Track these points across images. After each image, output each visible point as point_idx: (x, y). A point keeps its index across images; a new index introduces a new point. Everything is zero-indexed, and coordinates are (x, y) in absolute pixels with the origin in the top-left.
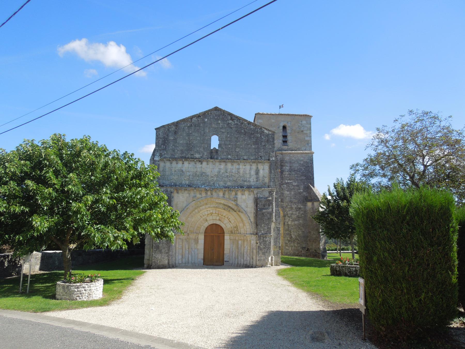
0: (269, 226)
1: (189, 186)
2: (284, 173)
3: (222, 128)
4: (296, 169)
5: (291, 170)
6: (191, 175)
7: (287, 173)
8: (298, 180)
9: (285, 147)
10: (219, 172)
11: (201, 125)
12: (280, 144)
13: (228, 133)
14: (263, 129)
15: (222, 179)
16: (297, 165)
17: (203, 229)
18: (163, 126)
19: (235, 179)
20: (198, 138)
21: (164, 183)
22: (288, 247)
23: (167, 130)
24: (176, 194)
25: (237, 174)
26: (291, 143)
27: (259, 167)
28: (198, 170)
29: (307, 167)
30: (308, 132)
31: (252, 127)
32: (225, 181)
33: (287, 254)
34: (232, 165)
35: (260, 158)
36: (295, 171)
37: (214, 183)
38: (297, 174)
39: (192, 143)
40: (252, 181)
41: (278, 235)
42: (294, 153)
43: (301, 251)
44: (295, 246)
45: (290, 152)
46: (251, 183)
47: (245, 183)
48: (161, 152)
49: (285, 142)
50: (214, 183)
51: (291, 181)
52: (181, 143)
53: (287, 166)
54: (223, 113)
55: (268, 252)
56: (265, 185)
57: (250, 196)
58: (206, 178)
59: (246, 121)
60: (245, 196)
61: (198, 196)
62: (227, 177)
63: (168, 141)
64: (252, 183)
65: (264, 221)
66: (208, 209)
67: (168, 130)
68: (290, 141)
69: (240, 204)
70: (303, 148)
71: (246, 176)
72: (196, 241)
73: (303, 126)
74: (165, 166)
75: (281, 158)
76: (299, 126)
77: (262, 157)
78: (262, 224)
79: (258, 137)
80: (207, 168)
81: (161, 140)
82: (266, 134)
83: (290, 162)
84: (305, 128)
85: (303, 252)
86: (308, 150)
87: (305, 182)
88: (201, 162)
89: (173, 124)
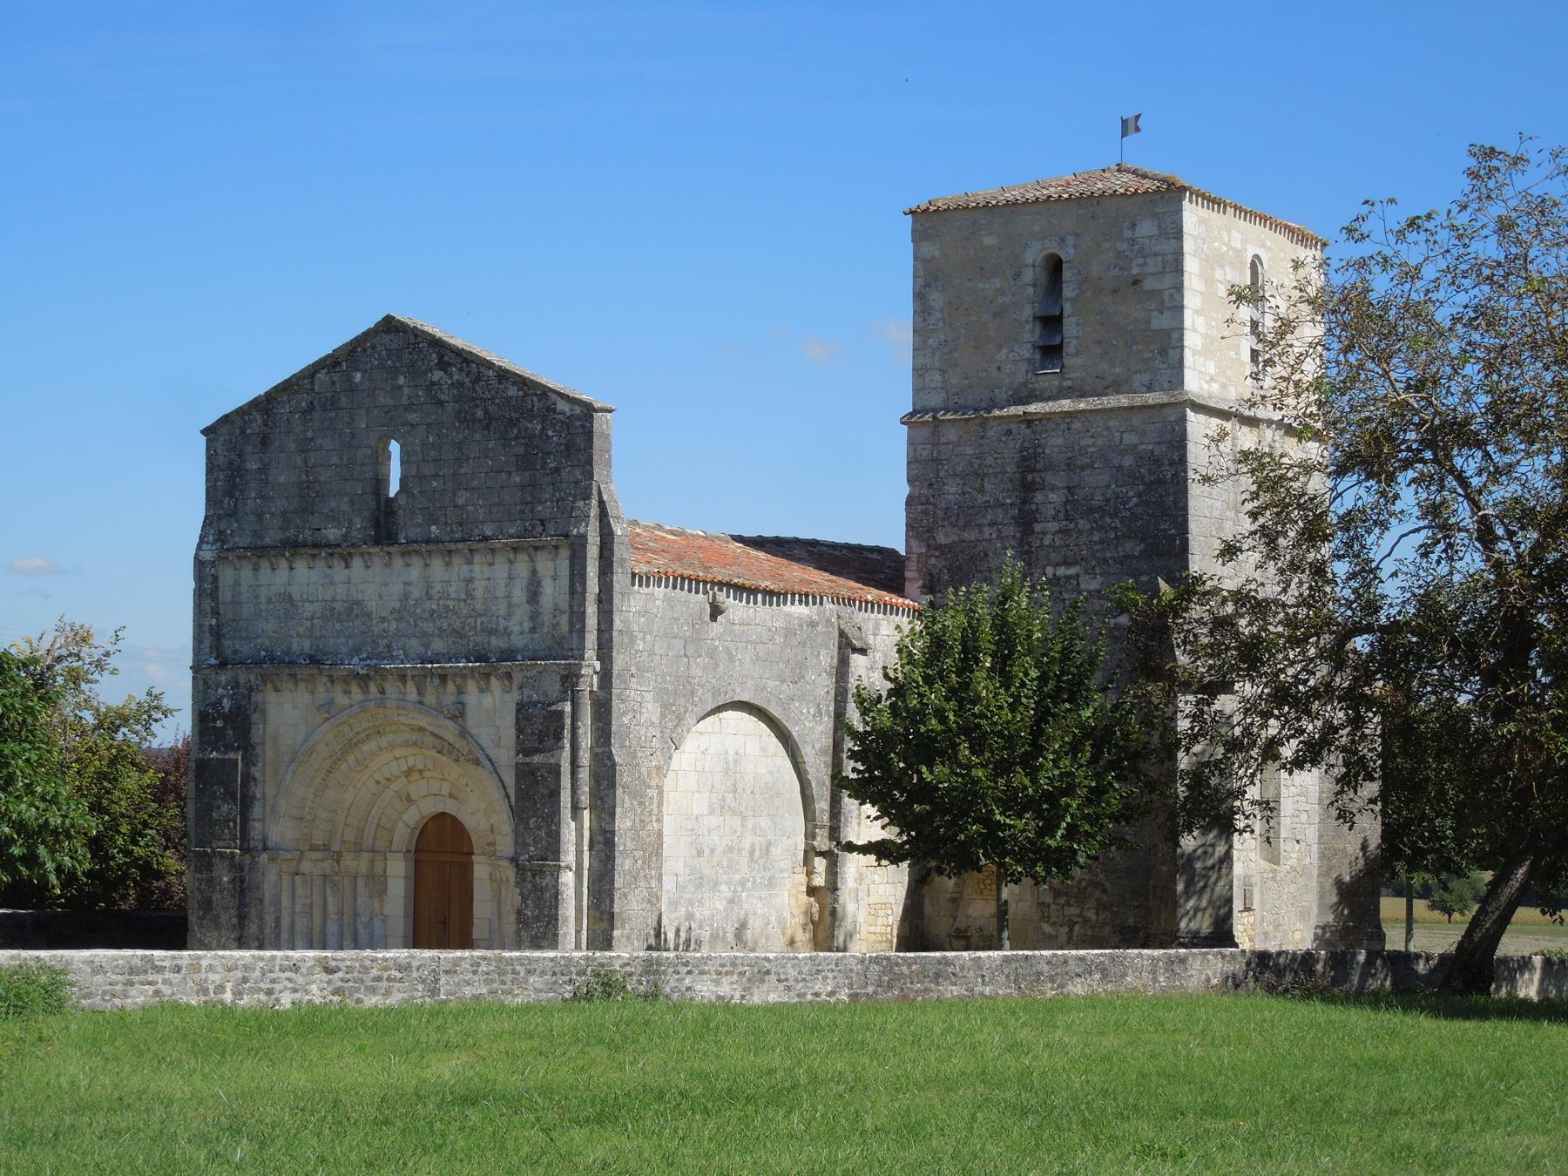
0: (554, 828)
1: (314, 661)
2: (1038, 527)
3: (408, 408)
4: (1098, 499)
5: (1070, 510)
6: (318, 615)
7: (1053, 526)
8: (1106, 561)
9: (1050, 376)
10: (406, 597)
11: (344, 400)
12: (1024, 367)
13: (429, 425)
14: (553, 396)
15: (416, 626)
17: (403, 836)
18: (225, 419)
19: (457, 625)
20: (335, 460)
21: (235, 652)
22: (1054, 924)
23: (237, 432)
24: (274, 693)
25: (465, 601)
26: (1077, 353)
27: (539, 569)
28: (339, 591)
29: (1152, 483)
30: (1168, 281)
31: (512, 391)
32: (424, 634)
34: (447, 564)
35: (539, 529)
36: (1091, 510)
37: (389, 646)
38: (1102, 528)
39: (316, 480)
40: (516, 629)
41: (606, 866)
44: (1086, 921)
45: (1066, 404)
46: (512, 637)
48: (223, 526)
50: (389, 646)
51: (1072, 571)
52: (280, 484)
54: (412, 340)
56: (563, 648)
57: (508, 697)
58: (363, 624)
59: (490, 365)
60: (492, 695)
61: (341, 699)
62: (432, 615)
63: (241, 477)
64: (518, 641)
65: (535, 803)
66: (398, 752)
67: (243, 432)
68: (1074, 342)
69: (474, 731)
70: (1137, 380)
71: (494, 608)
72: (378, 884)
73: (1141, 251)
74: (237, 584)
75: (1026, 444)
78: (529, 818)
79: (532, 436)
80: (366, 582)
81: (221, 477)
82: (560, 417)
83: (1070, 466)
86: (1166, 385)
87: (1141, 574)
88: (347, 561)
89: (255, 404)
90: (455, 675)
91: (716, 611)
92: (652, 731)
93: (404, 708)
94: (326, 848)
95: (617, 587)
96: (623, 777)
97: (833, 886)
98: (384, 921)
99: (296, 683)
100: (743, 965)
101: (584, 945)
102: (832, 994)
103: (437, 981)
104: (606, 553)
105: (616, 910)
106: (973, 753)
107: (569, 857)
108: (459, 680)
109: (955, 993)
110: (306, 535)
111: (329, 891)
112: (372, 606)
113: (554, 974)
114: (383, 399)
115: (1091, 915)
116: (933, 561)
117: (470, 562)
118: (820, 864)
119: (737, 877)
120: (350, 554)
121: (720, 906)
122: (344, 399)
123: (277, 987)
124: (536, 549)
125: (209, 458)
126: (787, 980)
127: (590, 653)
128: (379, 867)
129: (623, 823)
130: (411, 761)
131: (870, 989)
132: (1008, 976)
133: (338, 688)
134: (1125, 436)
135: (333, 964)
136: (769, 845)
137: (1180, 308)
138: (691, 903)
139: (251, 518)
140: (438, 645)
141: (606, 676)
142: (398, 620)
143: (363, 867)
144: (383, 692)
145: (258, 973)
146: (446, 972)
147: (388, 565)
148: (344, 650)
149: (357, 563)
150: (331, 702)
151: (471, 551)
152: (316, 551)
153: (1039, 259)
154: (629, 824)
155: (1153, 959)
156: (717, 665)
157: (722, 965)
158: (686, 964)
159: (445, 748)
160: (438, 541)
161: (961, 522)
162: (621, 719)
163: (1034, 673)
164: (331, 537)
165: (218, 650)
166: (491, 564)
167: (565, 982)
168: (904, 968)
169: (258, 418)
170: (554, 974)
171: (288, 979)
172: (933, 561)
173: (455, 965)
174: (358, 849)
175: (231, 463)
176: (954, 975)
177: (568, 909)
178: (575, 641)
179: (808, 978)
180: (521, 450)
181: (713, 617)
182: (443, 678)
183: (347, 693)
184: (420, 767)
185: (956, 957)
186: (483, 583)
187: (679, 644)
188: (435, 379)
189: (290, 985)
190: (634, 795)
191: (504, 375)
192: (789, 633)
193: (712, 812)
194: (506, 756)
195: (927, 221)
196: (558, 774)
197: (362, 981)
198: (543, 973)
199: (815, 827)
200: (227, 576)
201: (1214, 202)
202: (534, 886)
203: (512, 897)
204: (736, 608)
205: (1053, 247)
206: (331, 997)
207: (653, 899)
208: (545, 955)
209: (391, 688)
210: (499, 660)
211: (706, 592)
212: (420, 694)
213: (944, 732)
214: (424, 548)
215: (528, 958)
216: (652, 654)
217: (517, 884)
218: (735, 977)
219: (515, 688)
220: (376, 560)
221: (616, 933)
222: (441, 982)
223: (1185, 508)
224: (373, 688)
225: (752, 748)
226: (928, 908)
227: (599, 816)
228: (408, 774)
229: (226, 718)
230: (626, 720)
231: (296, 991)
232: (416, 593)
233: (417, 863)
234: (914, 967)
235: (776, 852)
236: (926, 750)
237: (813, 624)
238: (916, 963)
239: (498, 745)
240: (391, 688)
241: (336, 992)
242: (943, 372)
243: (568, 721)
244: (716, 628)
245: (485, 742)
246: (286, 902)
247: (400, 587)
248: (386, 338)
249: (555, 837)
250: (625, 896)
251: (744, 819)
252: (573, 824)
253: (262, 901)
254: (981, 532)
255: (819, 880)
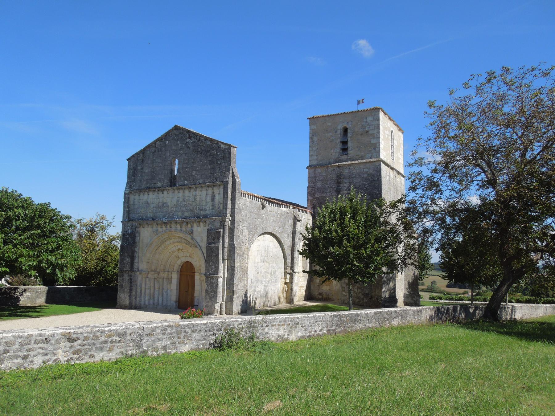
3: (180, 149)
9: (345, 157)
12: (338, 154)
14: (220, 143)
16: (360, 180)
17: (177, 267)
18: (133, 156)
19: (191, 208)
20: (161, 165)
21: (133, 218)
26: (352, 150)
29: (372, 181)
30: (376, 131)
31: (209, 143)
32: (183, 211)
33: (344, 302)
34: (189, 191)
35: (215, 180)
39: (156, 171)
42: (356, 164)
43: (363, 299)
45: (349, 162)
47: (201, 212)
48: (131, 184)
49: (345, 150)
53: (345, 183)
55: (215, 297)
57: (205, 228)
61: (160, 229)
64: (208, 212)
65: (211, 258)
66: (176, 244)
67: (137, 159)
68: (351, 147)
69: (195, 238)
70: (367, 156)
72: (169, 280)
73: (368, 124)
76: (362, 125)
77: (217, 179)
79: (213, 155)
82: (222, 149)
84: (371, 126)
85: (365, 300)
86: (375, 157)
90: (190, 222)
91: (263, 207)
92: (246, 238)
93: (176, 232)
94: (155, 271)
95: (237, 196)
96: (237, 251)
97: (291, 282)
98: (171, 291)
99: (148, 225)
100: (288, 321)
101: (224, 312)
102: (321, 330)
103: (141, 340)
104: (233, 187)
105: (235, 289)
106: (348, 243)
107: (221, 274)
108: (191, 223)
109: (361, 327)
110: (153, 185)
111: (156, 283)
112: (169, 204)
113: (206, 331)
114: (174, 148)
115: (356, 290)
116: (314, 201)
117: (196, 191)
118: (288, 276)
119: (267, 280)
120: (164, 190)
121: (263, 288)
122: (163, 148)
123: (32, 353)
124: (214, 186)
125: (128, 167)
126: (305, 326)
127: (229, 215)
128: (170, 276)
129: (237, 264)
130: (179, 247)
131: (334, 328)
132: (376, 320)
133: (159, 226)
134: (365, 170)
135: (74, 336)
136: (276, 271)
137: (379, 138)
138: (255, 287)
139: (139, 182)
140: (186, 214)
141: (233, 222)
142: (176, 207)
143: (166, 276)
144: (171, 227)
145: (17, 346)
146: (147, 335)
147: (173, 193)
148: (161, 216)
149: (165, 192)
150: (157, 230)
151: (196, 187)
152: (154, 189)
153: (341, 128)
154: (239, 264)
155: (414, 311)
156: (263, 222)
157: (281, 322)
158: (266, 322)
159: (188, 243)
160: (187, 185)
161: (322, 192)
162: (237, 234)
163: (363, 220)
164: (159, 186)
165: (129, 217)
166: (201, 191)
167: (211, 335)
168: (345, 318)
169: (141, 155)
170: (206, 331)
171: (40, 348)
172: (314, 201)
173: (153, 331)
174: (164, 271)
175: (134, 167)
176: (360, 320)
177: (220, 289)
178: (224, 211)
179: (313, 325)
180: (210, 159)
181: (263, 208)
182: (187, 223)
183: (162, 228)
184: (181, 248)
185: (361, 313)
186: (199, 196)
187: (253, 215)
188: (188, 141)
189: (42, 351)
190: (240, 256)
191: (206, 139)
192: (282, 215)
193: (261, 262)
194: (204, 245)
195: (313, 120)
196: (218, 249)
197: (94, 344)
198: (200, 331)
199: (287, 266)
200: (132, 197)
201: (385, 114)
202: (211, 282)
203: (205, 285)
204: (269, 207)
205: (345, 125)
206: (72, 356)
207: (245, 286)
208: (202, 322)
209: (173, 226)
210: (203, 218)
211: (261, 202)
212: (181, 227)
213: (337, 236)
214: (183, 187)
215: (193, 324)
216: (246, 217)
217: (206, 282)
218: (285, 327)
219: (207, 225)
220: (170, 191)
221: (234, 296)
222: (144, 341)
223: (381, 187)
224: (168, 226)
225: (272, 245)
226: (312, 288)
227: (230, 262)
228: (178, 250)
229: (129, 235)
230: (238, 234)
231: (46, 354)
232: (181, 200)
233: (180, 275)
234: (348, 318)
235: (277, 273)
236: (329, 242)
237: (287, 213)
238: (348, 316)
239: (202, 241)
240: (173, 226)
241: (76, 352)
242: (317, 156)
243: (222, 234)
244: (263, 211)
245: (198, 241)
246: (143, 286)
247: (176, 198)
248: (175, 131)
249: (217, 268)
250: (237, 285)
251: (269, 264)
252: (222, 264)
253: (137, 285)
254: (327, 194)
255: (288, 281)
